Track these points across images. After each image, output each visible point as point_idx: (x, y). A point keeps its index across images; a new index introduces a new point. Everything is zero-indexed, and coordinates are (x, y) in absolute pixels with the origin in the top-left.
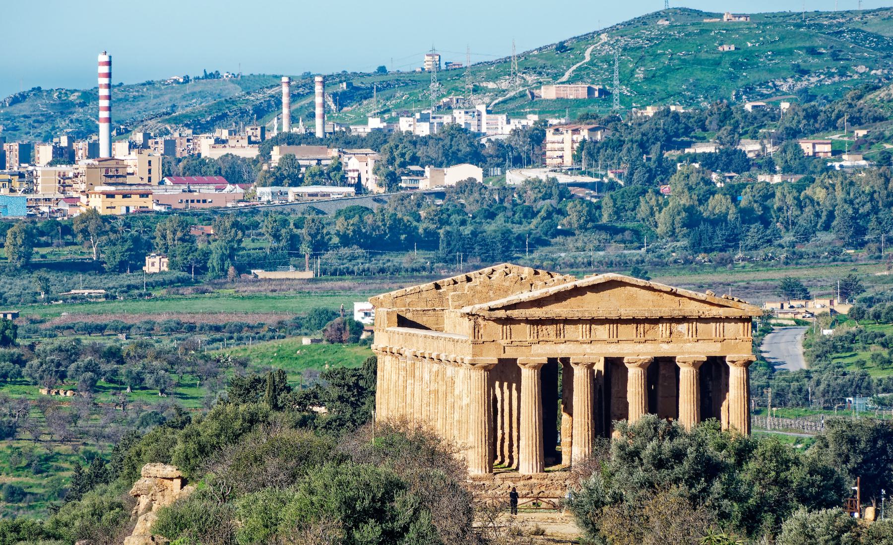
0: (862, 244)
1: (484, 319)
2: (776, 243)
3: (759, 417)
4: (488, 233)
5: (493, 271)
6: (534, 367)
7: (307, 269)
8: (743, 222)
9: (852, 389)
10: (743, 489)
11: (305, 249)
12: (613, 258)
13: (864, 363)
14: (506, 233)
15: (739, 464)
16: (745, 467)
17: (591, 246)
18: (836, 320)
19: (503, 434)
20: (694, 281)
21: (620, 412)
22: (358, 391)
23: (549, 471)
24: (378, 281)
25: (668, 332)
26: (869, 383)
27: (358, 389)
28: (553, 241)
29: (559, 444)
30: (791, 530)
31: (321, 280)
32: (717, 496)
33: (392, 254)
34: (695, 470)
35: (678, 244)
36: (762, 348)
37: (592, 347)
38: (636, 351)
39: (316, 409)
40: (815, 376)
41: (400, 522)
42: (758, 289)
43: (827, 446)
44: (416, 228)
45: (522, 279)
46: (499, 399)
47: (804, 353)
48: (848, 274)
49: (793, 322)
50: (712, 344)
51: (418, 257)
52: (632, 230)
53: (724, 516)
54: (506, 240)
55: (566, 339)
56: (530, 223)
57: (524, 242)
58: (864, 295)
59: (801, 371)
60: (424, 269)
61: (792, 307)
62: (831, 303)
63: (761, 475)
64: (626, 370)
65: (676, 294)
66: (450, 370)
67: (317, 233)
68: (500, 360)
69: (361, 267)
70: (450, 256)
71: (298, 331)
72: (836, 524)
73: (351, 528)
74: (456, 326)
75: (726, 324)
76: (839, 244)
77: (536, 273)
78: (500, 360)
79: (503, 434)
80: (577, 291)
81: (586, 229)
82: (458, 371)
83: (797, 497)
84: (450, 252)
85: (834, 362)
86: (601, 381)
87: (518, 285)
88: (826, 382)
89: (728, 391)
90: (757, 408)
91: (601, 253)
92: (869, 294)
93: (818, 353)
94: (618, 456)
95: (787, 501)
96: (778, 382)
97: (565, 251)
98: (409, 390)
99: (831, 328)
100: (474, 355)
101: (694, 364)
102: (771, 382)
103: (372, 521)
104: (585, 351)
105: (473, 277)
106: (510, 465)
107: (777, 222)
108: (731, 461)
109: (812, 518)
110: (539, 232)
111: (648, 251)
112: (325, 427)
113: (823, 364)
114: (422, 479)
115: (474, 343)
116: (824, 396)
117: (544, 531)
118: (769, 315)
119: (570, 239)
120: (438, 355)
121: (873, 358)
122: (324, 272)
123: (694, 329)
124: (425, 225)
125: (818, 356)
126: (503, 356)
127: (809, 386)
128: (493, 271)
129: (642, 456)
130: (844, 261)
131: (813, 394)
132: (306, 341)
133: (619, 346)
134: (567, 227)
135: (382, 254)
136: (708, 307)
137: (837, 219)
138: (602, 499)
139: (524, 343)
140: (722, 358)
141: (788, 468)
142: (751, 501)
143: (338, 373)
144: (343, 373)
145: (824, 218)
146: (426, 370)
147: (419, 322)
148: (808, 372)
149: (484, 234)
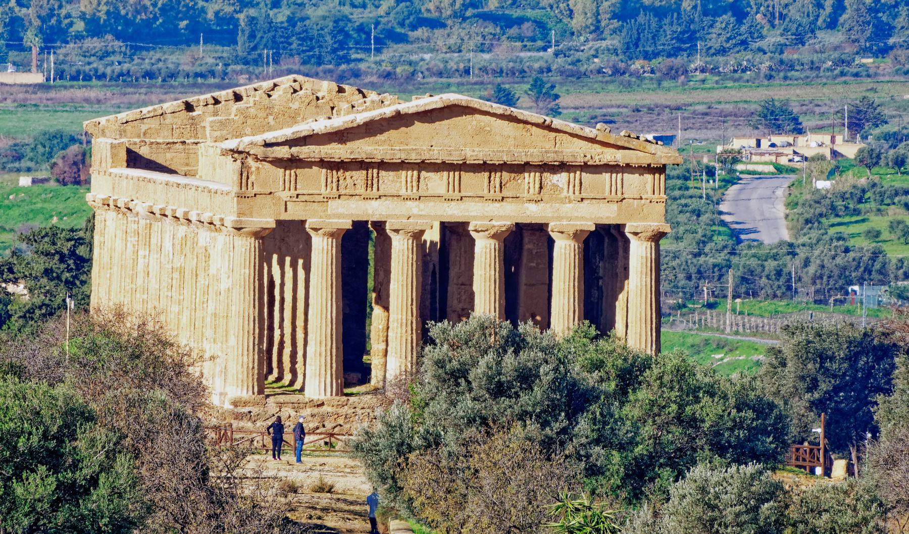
0: (884, 51)
1: (257, 159)
2: (754, 46)
3: (714, 312)
4: (314, 19)
5: (275, 85)
6: (332, 235)
7: (34, 69)
8: (705, 13)
9: (859, 274)
10: (624, 431)
11: (32, 39)
12: (504, 65)
13: (878, 234)
14: (340, 21)
15: (622, 393)
16: (631, 397)
17: (472, 44)
18: (837, 166)
19: (282, 335)
20: (625, 103)
21: (461, 306)
22: (75, 263)
23: (351, 395)
24: (143, 90)
25: (537, 186)
26: (884, 265)
27: (71, 261)
28: (413, 35)
29: (368, 353)
30: (684, 497)
31: (55, 87)
32: (584, 440)
33: (165, 48)
34: (553, 400)
35: (604, 44)
36: (723, 207)
37: (422, 206)
38: (489, 214)
39: (11, 288)
40: (802, 253)
41: (85, 471)
42: (724, 116)
43: (784, 365)
44: (203, 10)
45: (318, 99)
46: (277, 282)
47: (787, 216)
48: (860, 96)
49: (771, 169)
50: (603, 205)
51: (205, 54)
52: (535, 21)
53: (593, 471)
54: (342, 31)
55: (381, 192)
56: (377, 7)
57: (368, 34)
58: (885, 128)
59: (781, 244)
60: (213, 73)
61: (773, 145)
62: (833, 141)
63: (656, 410)
64: (473, 241)
65: (549, 128)
66: (204, 236)
67: (51, 15)
68: (279, 223)
69: (117, 68)
70: (254, 55)
71: (17, 165)
72: (753, 489)
73: (9, 479)
74: (215, 170)
75: (626, 175)
76: (849, 49)
77: (341, 90)
78: (279, 223)
79: (282, 335)
80: (400, 120)
81: (465, 19)
82: (215, 239)
83: (711, 445)
84: (255, 48)
85: (832, 231)
86: (436, 258)
87: (312, 108)
88: (818, 262)
89: (627, 277)
90: (712, 300)
91: (486, 56)
92: (891, 127)
93: (808, 216)
94: (434, 376)
95: (694, 450)
96: (744, 260)
97: (432, 50)
98: (140, 267)
99: (828, 179)
100: (240, 214)
101: (576, 235)
102: (735, 260)
103: (42, 469)
104: (411, 212)
105: (244, 94)
106: (292, 383)
107: (757, 13)
108: (612, 386)
109: (715, 479)
110: (391, 22)
111: (556, 55)
112: (24, 317)
113: (814, 234)
114: (131, 404)
115: (240, 196)
116: (814, 283)
117: (332, 487)
118: (734, 158)
119: (438, 32)
120: (186, 213)
121: (891, 227)
122: (61, 75)
123: (577, 182)
124: (217, 7)
125: (807, 221)
126: (284, 217)
127: (793, 266)
128: (275, 85)
129: (471, 377)
130: (856, 75)
131: (800, 279)
132: (25, 181)
133: (462, 205)
134: (435, 15)
135: (147, 49)
136: (598, 148)
137: (849, 11)
138: (407, 440)
139: (317, 198)
140: (620, 228)
141: (697, 400)
142: (639, 450)
143: (47, 235)
144: (53, 234)
145: (828, 10)
146: (168, 234)
147: (160, 160)
148: (791, 245)
149: (307, 22)
